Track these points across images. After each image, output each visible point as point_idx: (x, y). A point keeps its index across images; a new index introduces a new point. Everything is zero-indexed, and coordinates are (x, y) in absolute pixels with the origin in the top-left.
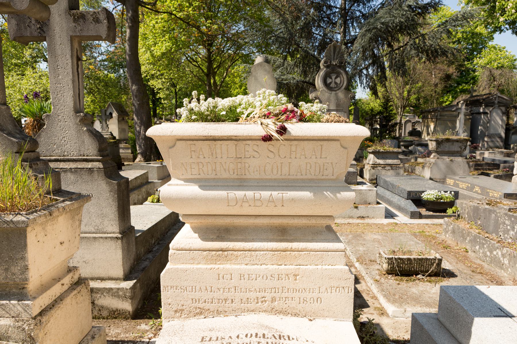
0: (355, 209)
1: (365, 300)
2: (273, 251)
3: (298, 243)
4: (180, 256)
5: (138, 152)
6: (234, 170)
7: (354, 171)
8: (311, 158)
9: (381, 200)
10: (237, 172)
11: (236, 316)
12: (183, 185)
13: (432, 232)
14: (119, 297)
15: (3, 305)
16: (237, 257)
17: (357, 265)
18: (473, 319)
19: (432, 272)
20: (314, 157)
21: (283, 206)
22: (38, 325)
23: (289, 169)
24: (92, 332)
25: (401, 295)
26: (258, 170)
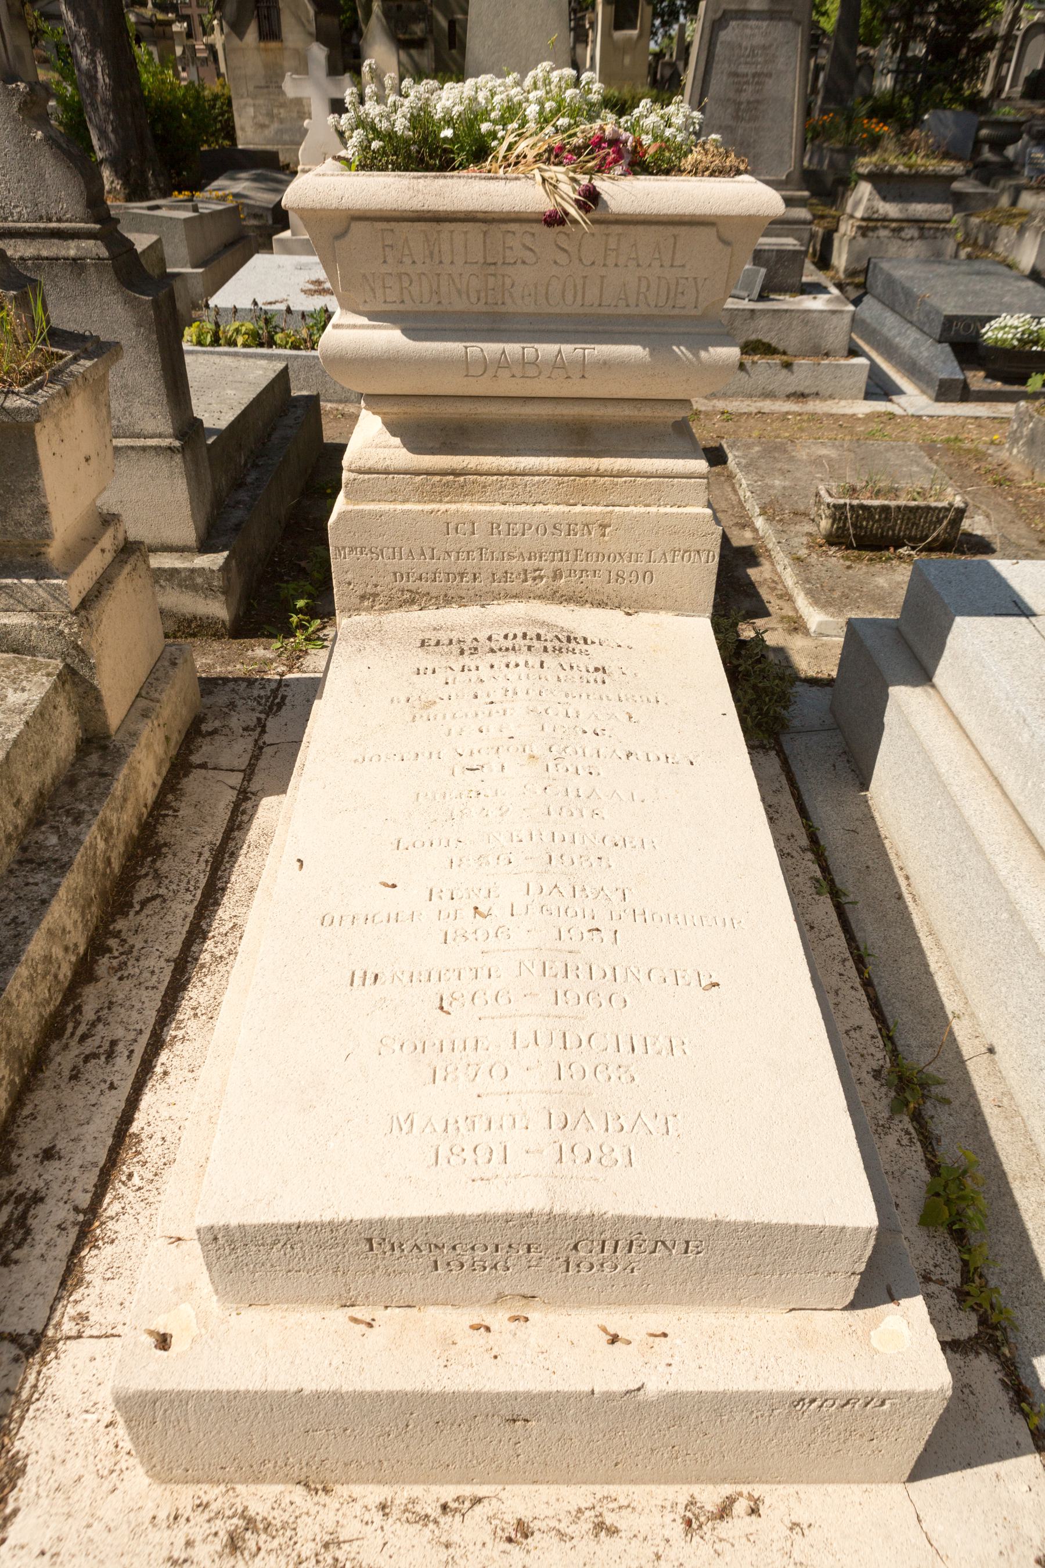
0: (784, 371)
1: (762, 601)
2: (560, 476)
3: (613, 460)
4: (366, 484)
5: (100, 155)
6: (478, 292)
7: (798, 248)
8: (650, 265)
9: (868, 342)
10: (487, 296)
11: (483, 606)
12: (368, 327)
13: (975, 438)
14: (195, 588)
15: (7, 586)
16: (485, 487)
17: (759, 522)
18: (953, 620)
19: (934, 540)
20: (656, 264)
21: (583, 377)
22: (86, 625)
23: (601, 290)
24: (167, 655)
25: (847, 591)
26: (533, 293)
